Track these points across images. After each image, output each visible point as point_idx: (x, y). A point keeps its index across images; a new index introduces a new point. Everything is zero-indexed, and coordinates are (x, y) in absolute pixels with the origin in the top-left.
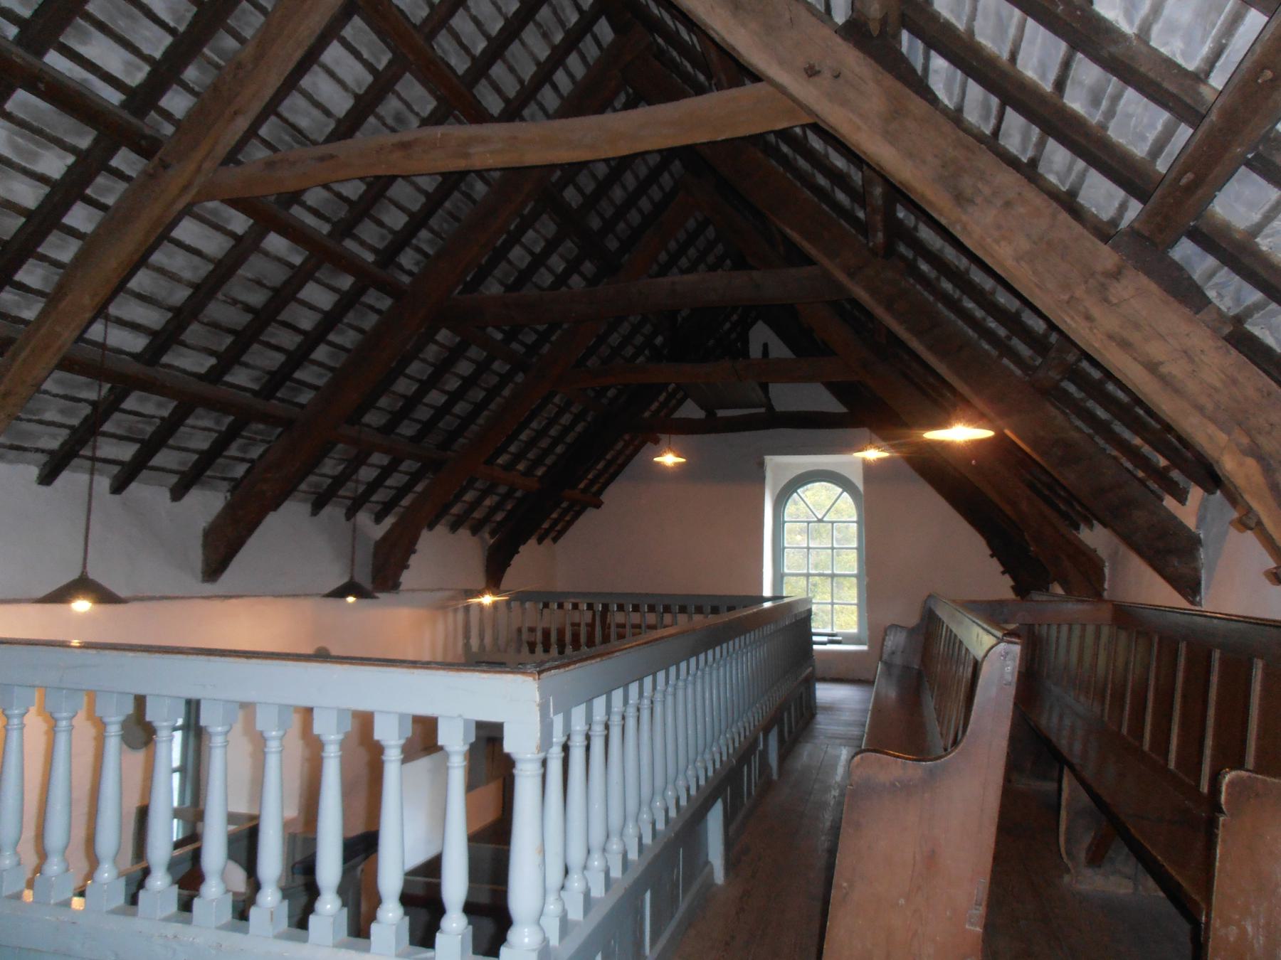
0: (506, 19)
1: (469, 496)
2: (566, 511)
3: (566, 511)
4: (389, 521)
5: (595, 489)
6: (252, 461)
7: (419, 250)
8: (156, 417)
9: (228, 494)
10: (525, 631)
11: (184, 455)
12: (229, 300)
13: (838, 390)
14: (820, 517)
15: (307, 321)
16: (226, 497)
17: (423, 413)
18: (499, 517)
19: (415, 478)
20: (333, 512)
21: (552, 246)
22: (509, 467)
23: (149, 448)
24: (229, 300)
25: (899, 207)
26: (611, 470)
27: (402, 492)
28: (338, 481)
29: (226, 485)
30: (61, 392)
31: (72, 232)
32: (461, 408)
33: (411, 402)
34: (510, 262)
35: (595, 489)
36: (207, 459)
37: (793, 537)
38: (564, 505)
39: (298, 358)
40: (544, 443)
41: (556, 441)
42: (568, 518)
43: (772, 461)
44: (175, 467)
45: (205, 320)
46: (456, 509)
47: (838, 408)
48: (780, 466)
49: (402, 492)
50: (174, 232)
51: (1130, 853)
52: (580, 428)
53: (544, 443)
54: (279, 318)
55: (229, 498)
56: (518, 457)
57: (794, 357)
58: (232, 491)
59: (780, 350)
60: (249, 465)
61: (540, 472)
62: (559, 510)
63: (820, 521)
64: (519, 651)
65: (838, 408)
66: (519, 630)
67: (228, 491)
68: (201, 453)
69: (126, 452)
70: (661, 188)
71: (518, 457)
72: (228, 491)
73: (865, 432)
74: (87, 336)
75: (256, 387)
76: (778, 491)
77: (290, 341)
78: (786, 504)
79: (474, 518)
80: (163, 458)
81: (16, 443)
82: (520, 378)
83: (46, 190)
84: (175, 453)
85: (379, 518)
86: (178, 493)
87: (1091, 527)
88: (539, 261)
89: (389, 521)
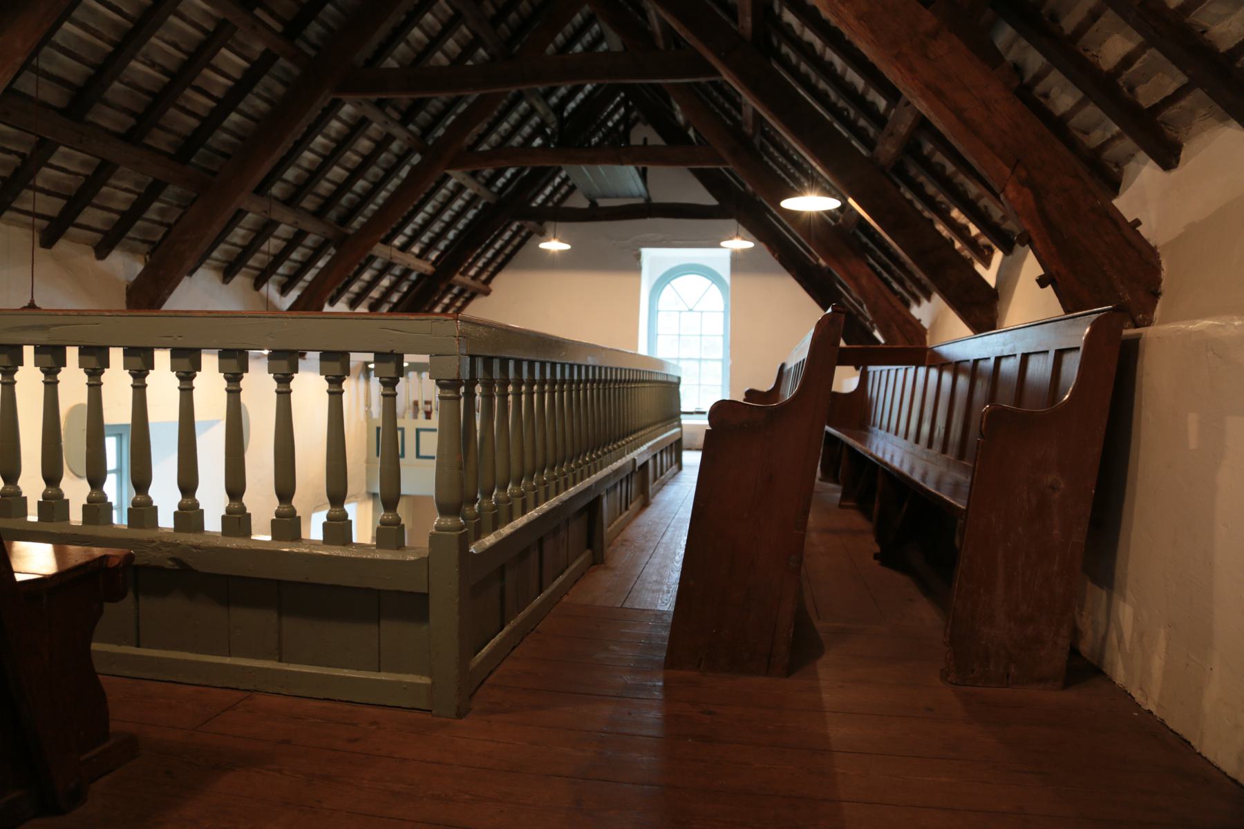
1: (367, 276)
2: (456, 297)
3: (456, 297)
5: (484, 277)
6: (169, 225)
7: (323, 24)
8: (82, 175)
9: (148, 257)
10: (421, 405)
11: (105, 214)
12: (148, 62)
13: (709, 180)
14: (691, 308)
16: (146, 260)
17: (325, 187)
18: (395, 298)
19: (317, 253)
20: (241, 281)
23: (76, 202)
24: (148, 62)
26: (499, 260)
28: (248, 250)
29: (146, 248)
32: (361, 185)
33: (315, 174)
34: (408, 43)
35: (484, 277)
36: (128, 219)
37: (663, 321)
38: (455, 291)
39: (212, 121)
40: (437, 227)
41: (449, 226)
42: (458, 304)
43: (648, 254)
44: (99, 226)
45: (126, 80)
46: (355, 288)
47: (709, 200)
48: (654, 259)
52: (471, 214)
53: (437, 227)
54: (194, 83)
55: (148, 260)
56: (412, 240)
58: (151, 253)
59: (655, 139)
60: (166, 229)
61: (433, 256)
62: (450, 296)
63: (691, 310)
64: (415, 417)
65: (709, 200)
66: (416, 404)
67: (148, 253)
68: (122, 213)
69: (52, 206)
71: (412, 240)
72: (148, 253)
73: (733, 223)
75: (171, 151)
76: (653, 282)
77: (203, 103)
78: (663, 288)
79: (371, 298)
80: (90, 216)
84: (99, 213)
85: (284, 290)
86: (102, 251)
87: (919, 303)
88: (436, 41)
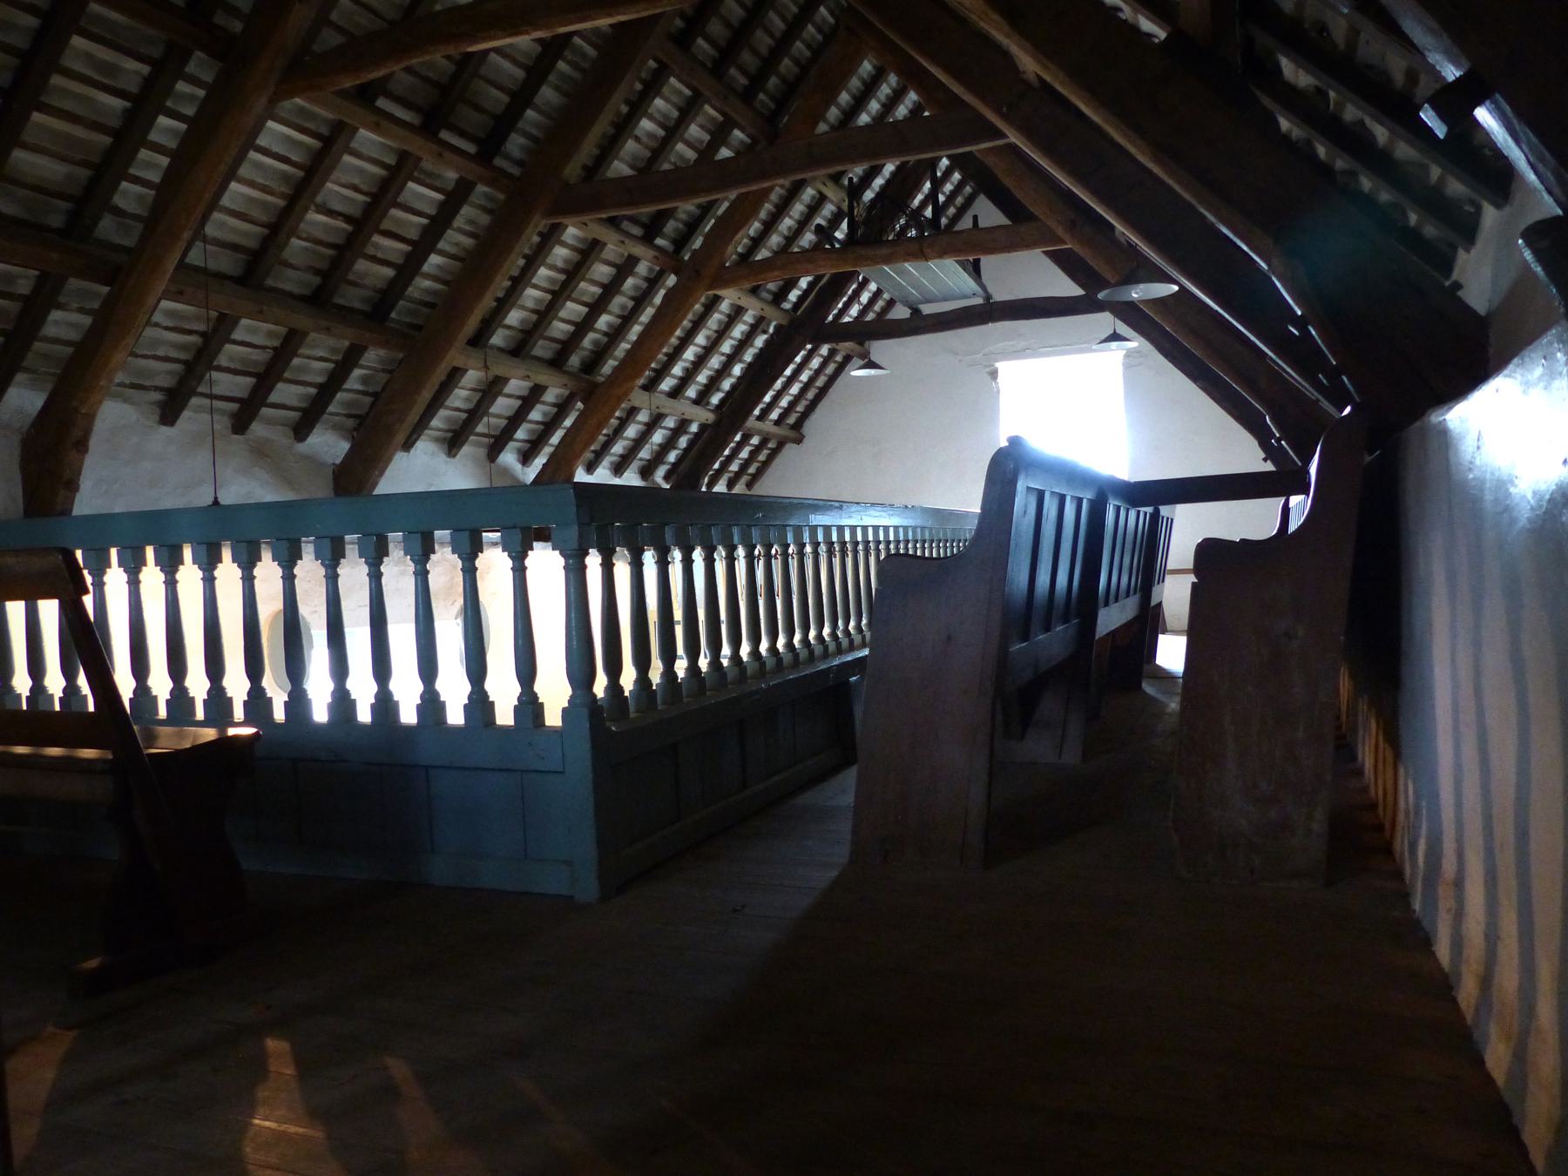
0: (358, 543)
4: (539, 462)
13: (1067, 263)
15: (413, 224)
21: (687, 111)
22: (675, 393)
25: (610, 174)
27: (549, 426)
30: (170, 324)
31: (158, 148)
32: (604, 321)
41: (731, 359)
44: (295, 403)
45: (304, 236)
46: (618, 448)
49: (549, 426)
50: (549, 258)
51: (560, 284)
52: (760, 341)
57: (1010, 223)
61: (715, 399)
70: (755, 52)
74: (188, 260)
81: (136, 381)
82: (671, 280)
83: (400, 199)
85: (526, 457)
88: (673, 130)
89: (539, 462)
